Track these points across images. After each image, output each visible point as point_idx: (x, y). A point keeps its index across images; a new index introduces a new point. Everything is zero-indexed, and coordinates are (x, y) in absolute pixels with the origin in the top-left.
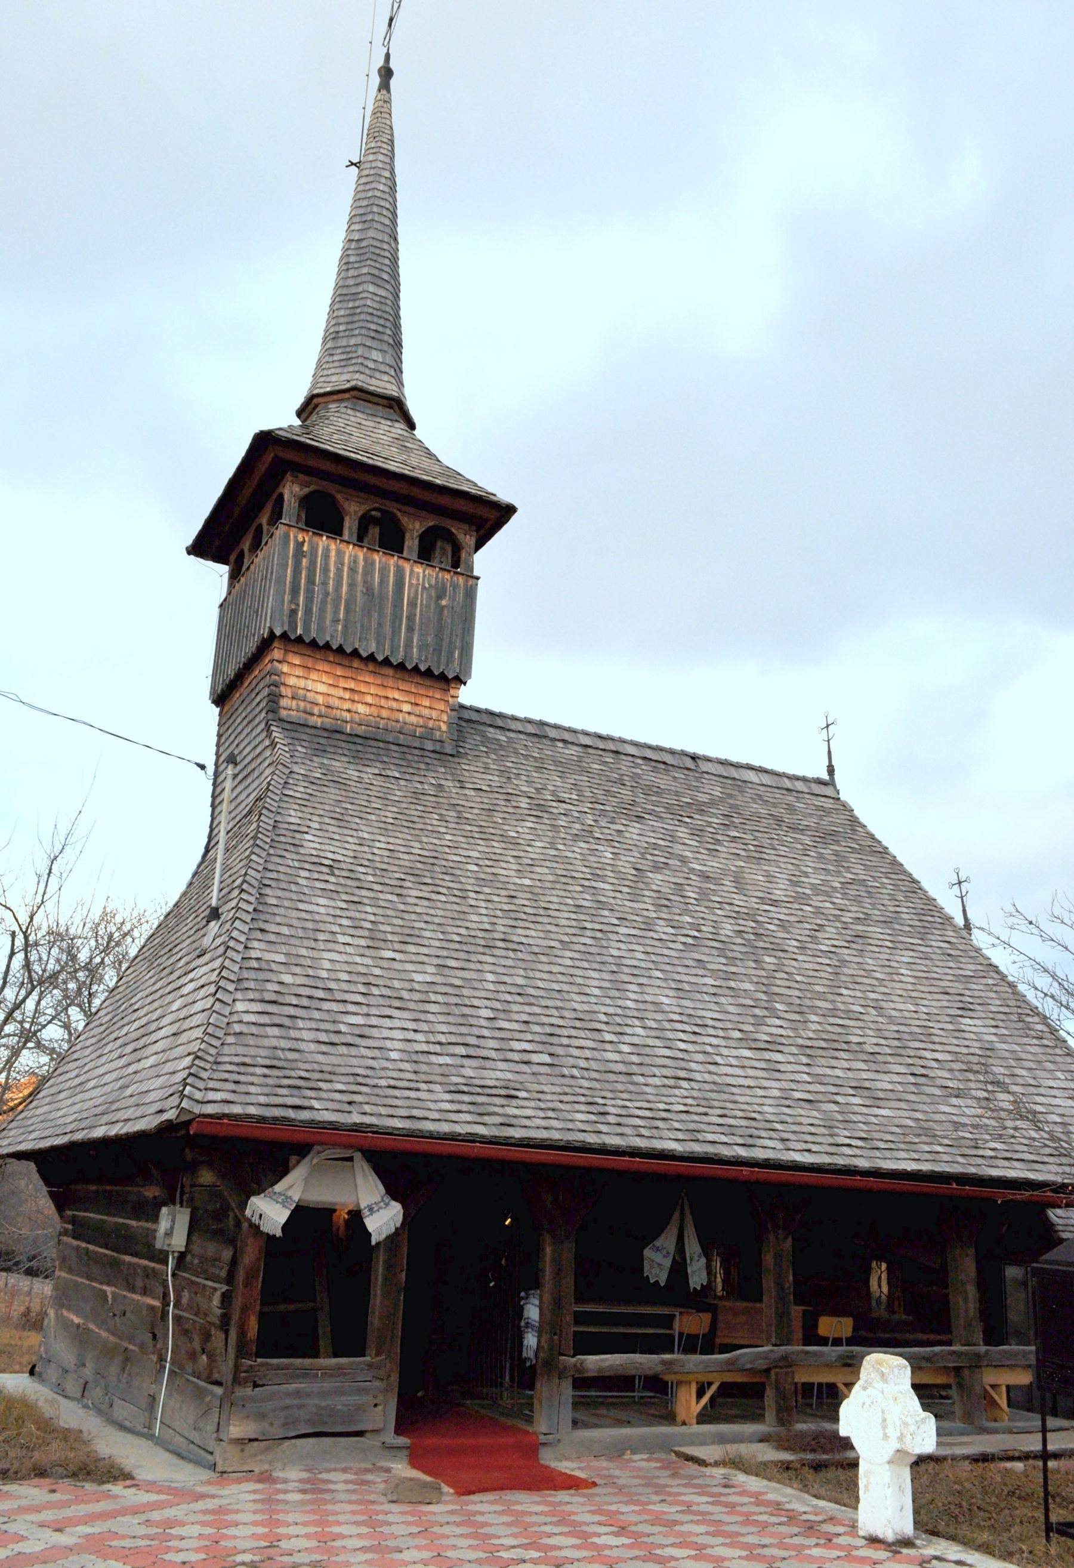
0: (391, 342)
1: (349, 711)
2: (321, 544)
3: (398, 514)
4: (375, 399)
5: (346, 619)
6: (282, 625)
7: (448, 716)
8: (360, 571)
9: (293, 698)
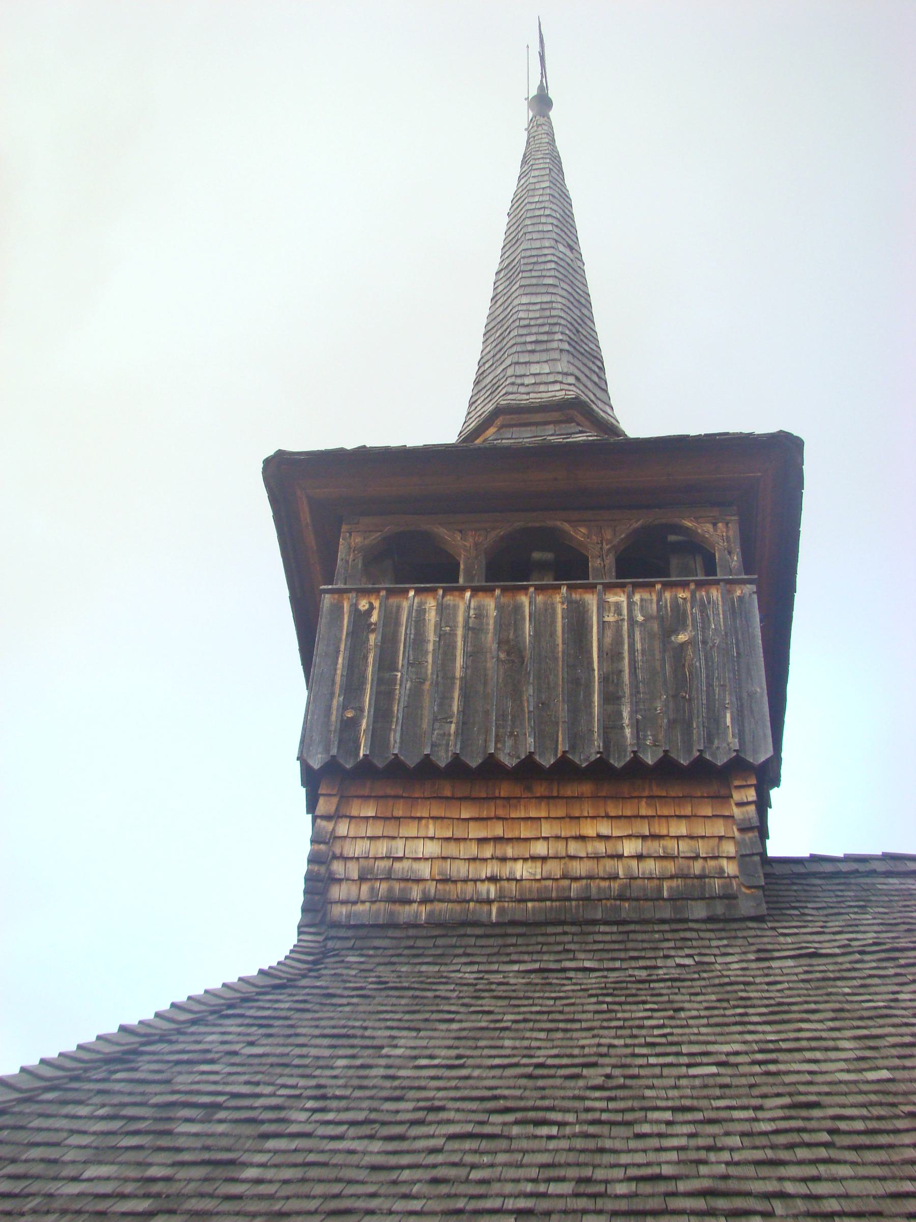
0: (566, 346)
1: (493, 879)
2: (405, 604)
3: (566, 526)
4: (538, 417)
5: (465, 711)
6: (327, 750)
7: (737, 844)
8: (491, 627)
9: (362, 879)
